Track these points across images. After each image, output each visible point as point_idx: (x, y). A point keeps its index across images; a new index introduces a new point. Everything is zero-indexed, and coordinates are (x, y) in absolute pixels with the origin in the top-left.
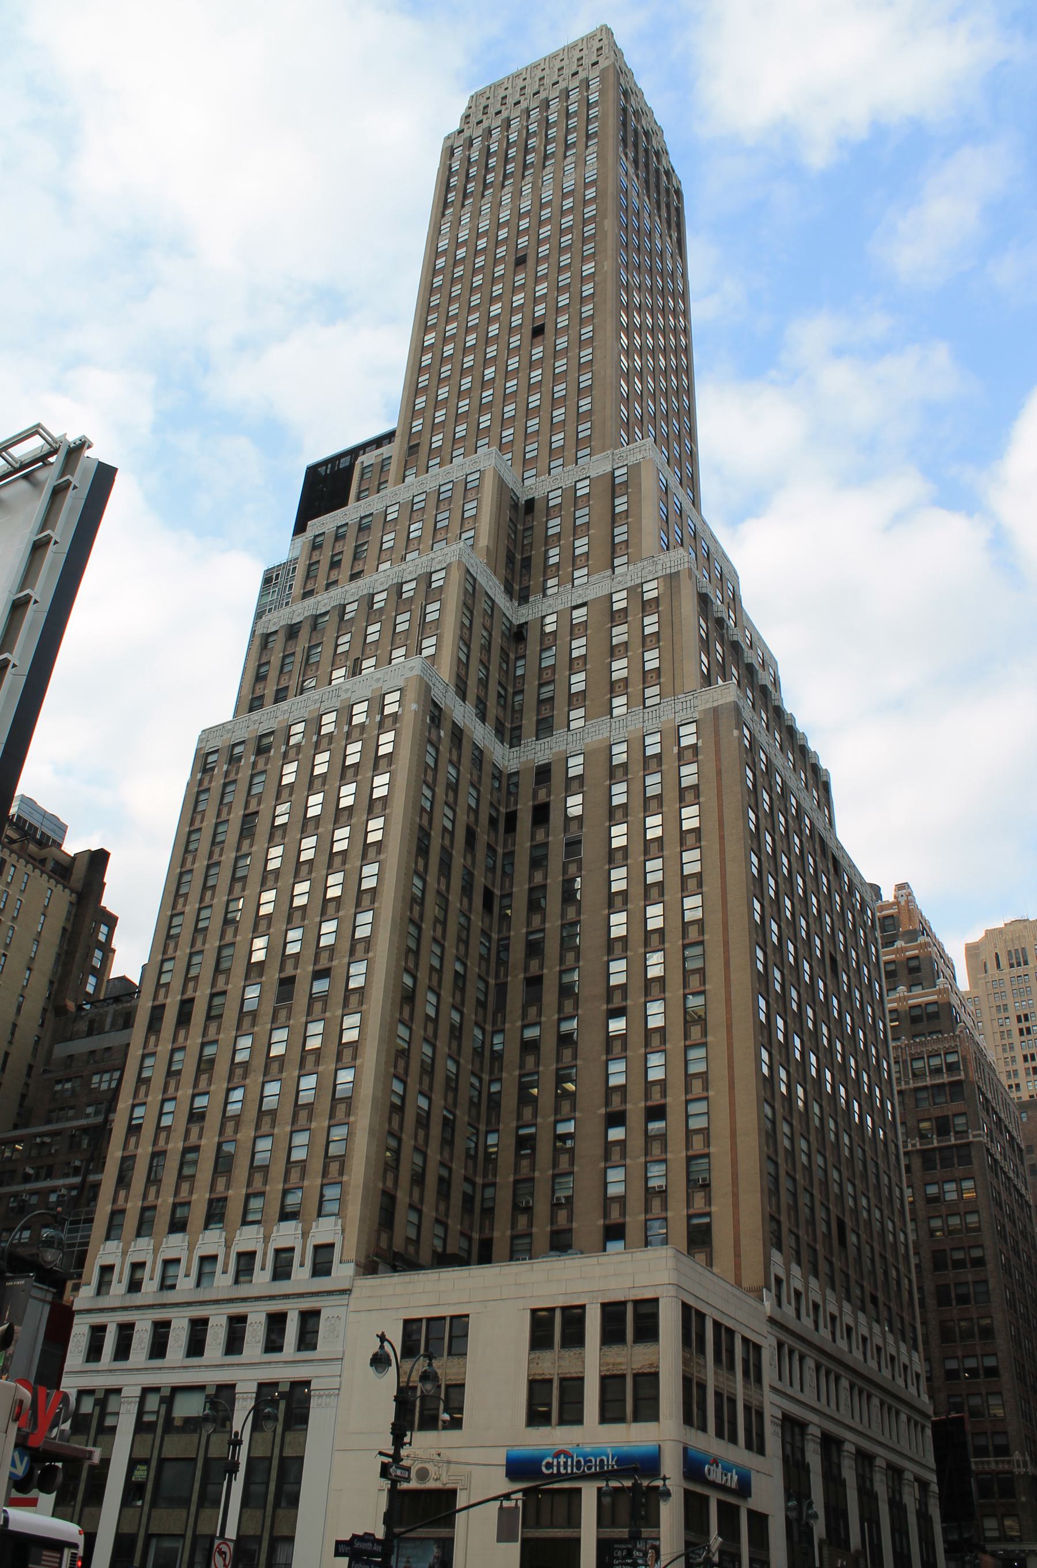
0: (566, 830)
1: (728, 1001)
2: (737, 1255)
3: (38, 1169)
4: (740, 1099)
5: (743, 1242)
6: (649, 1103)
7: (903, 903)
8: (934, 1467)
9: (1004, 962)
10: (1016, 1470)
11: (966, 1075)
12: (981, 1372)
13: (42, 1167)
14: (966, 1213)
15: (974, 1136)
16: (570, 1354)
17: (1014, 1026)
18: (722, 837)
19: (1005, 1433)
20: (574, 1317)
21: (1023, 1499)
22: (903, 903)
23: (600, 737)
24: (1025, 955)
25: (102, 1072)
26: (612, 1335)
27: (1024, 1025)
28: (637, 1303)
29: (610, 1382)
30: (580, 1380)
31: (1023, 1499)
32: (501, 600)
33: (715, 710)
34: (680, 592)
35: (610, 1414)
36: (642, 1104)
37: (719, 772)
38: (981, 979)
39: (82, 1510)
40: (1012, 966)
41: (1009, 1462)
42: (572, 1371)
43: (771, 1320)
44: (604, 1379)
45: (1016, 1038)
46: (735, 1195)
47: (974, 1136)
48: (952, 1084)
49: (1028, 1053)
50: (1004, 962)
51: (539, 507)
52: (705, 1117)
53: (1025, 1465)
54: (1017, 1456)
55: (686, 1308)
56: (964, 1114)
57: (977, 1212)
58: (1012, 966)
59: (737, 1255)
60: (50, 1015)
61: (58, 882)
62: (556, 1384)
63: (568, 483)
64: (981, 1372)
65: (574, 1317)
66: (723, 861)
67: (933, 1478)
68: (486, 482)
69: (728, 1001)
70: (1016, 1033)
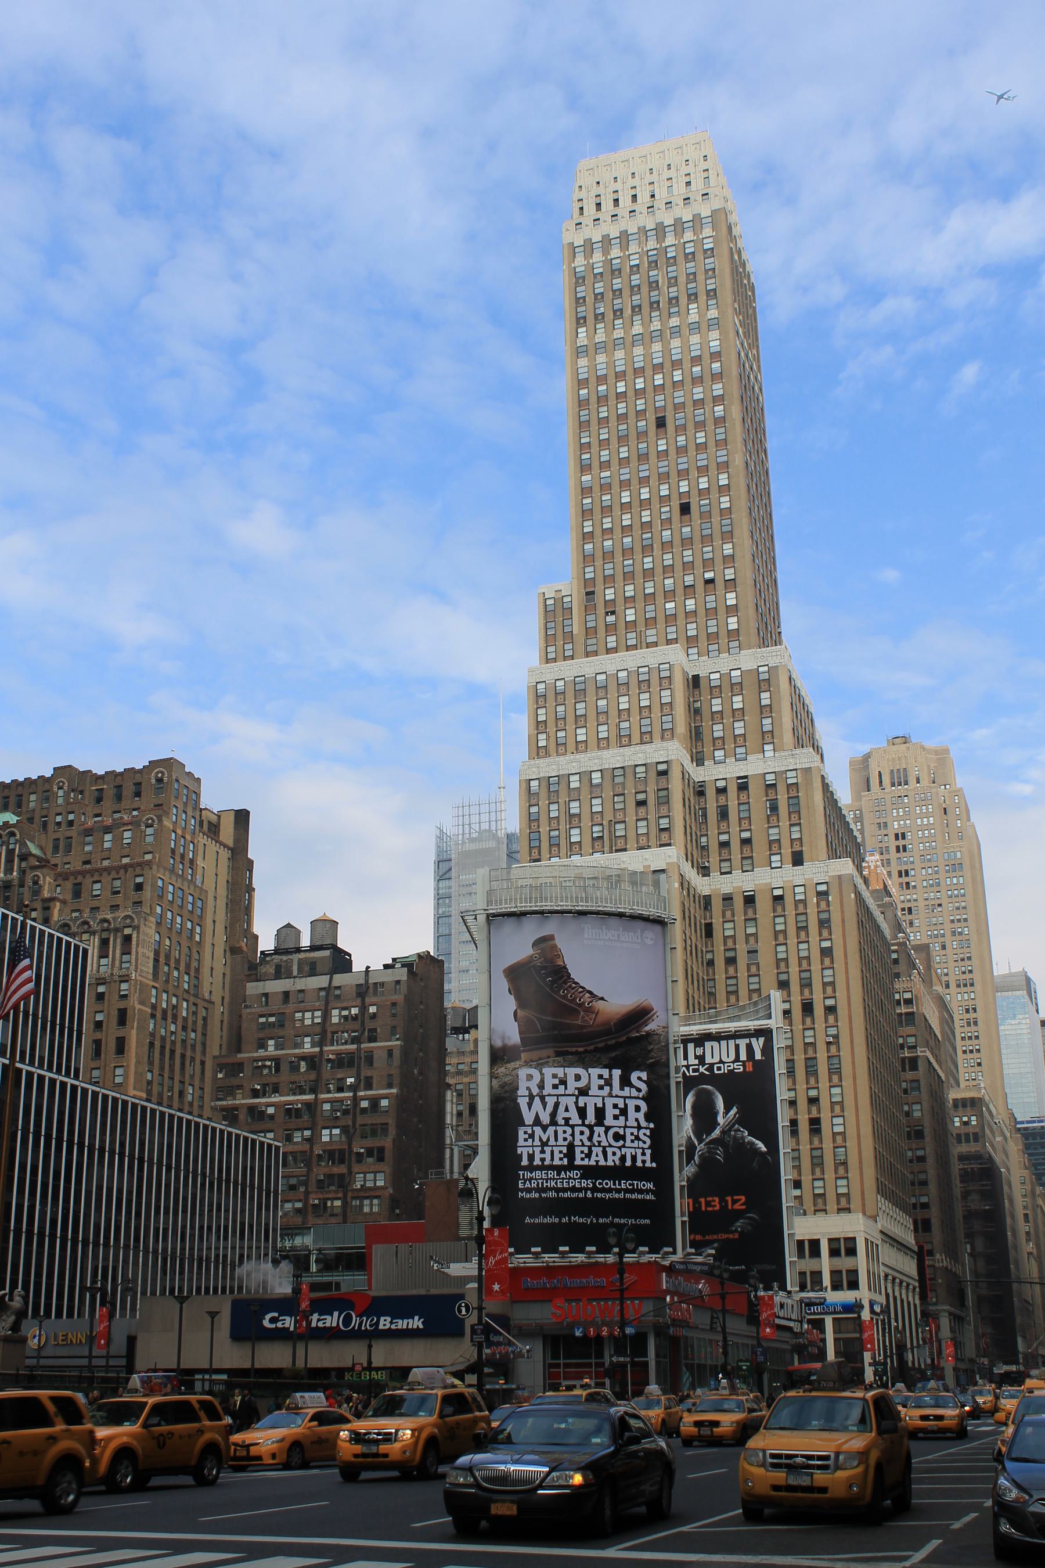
0: (747, 942)
1: (853, 1063)
2: (863, 1199)
3: (264, 1086)
4: (861, 1117)
5: (866, 1193)
6: (811, 1116)
7: (872, 867)
8: (917, 1278)
9: (886, 780)
10: (937, 1265)
11: (917, 1009)
12: (918, 1206)
13: (268, 1084)
14: (913, 1103)
15: (921, 1052)
16: (815, 1260)
17: (893, 844)
18: (846, 963)
19: (932, 1243)
20: (815, 1244)
21: (940, 1281)
22: (872, 867)
23: (764, 882)
24: (906, 776)
25: (304, 1012)
26: (834, 1253)
27: (901, 843)
28: (846, 1239)
29: (835, 1273)
30: (820, 1273)
31: (940, 1281)
32: (690, 767)
33: (840, 877)
34: (812, 784)
35: (836, 1286)
36: (807, 1116)
37: (843, 921)
38: (864, 796)
39: (26, 1303)
40: (893, 785)
41: (932, 1260)
42: (816, 1269)
43: (881, 1232)
44: (832, 1272)
45: (893, 855)
46: (861, 1169)
47: (921, 1052)
48: (907, 1014)
49: (903, 868)
50: (886, 780)
51: (703, 683)
52: (842, 1126)
53: (942, 1262)
54: (938, 1256)
55: (866, 1240)
56: (914, 1036)
57: (920, 1103)
58: (893, 785)
59: (863, 1199)
60: (228, 954)
61: (212, 839)
62: (808, 1274)
63: (725, 670)
64: (918, 1206)
65: (815, 1244)
66: (847, 978)
67: (917, 1284)
68: (676, 672)
69: (853, 1063)
70: (893, 849)
